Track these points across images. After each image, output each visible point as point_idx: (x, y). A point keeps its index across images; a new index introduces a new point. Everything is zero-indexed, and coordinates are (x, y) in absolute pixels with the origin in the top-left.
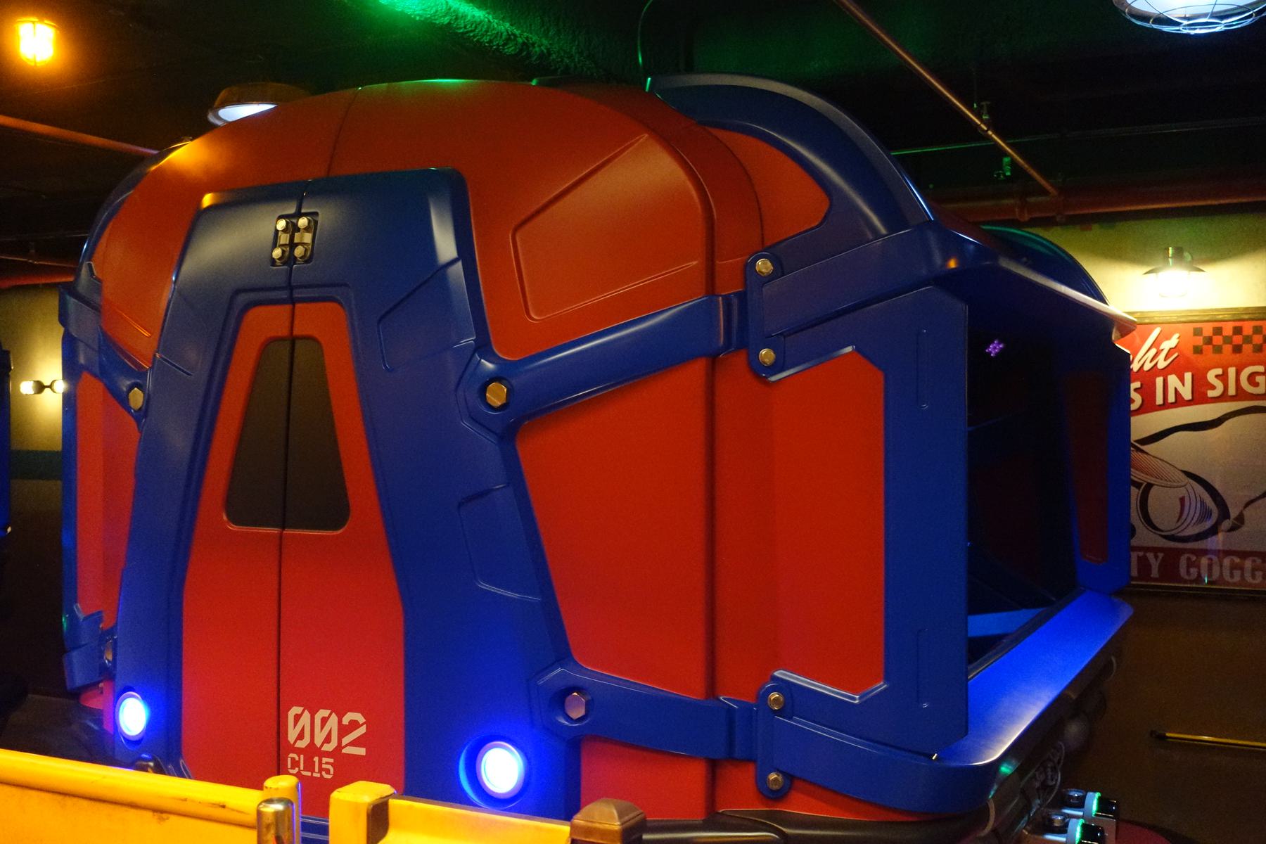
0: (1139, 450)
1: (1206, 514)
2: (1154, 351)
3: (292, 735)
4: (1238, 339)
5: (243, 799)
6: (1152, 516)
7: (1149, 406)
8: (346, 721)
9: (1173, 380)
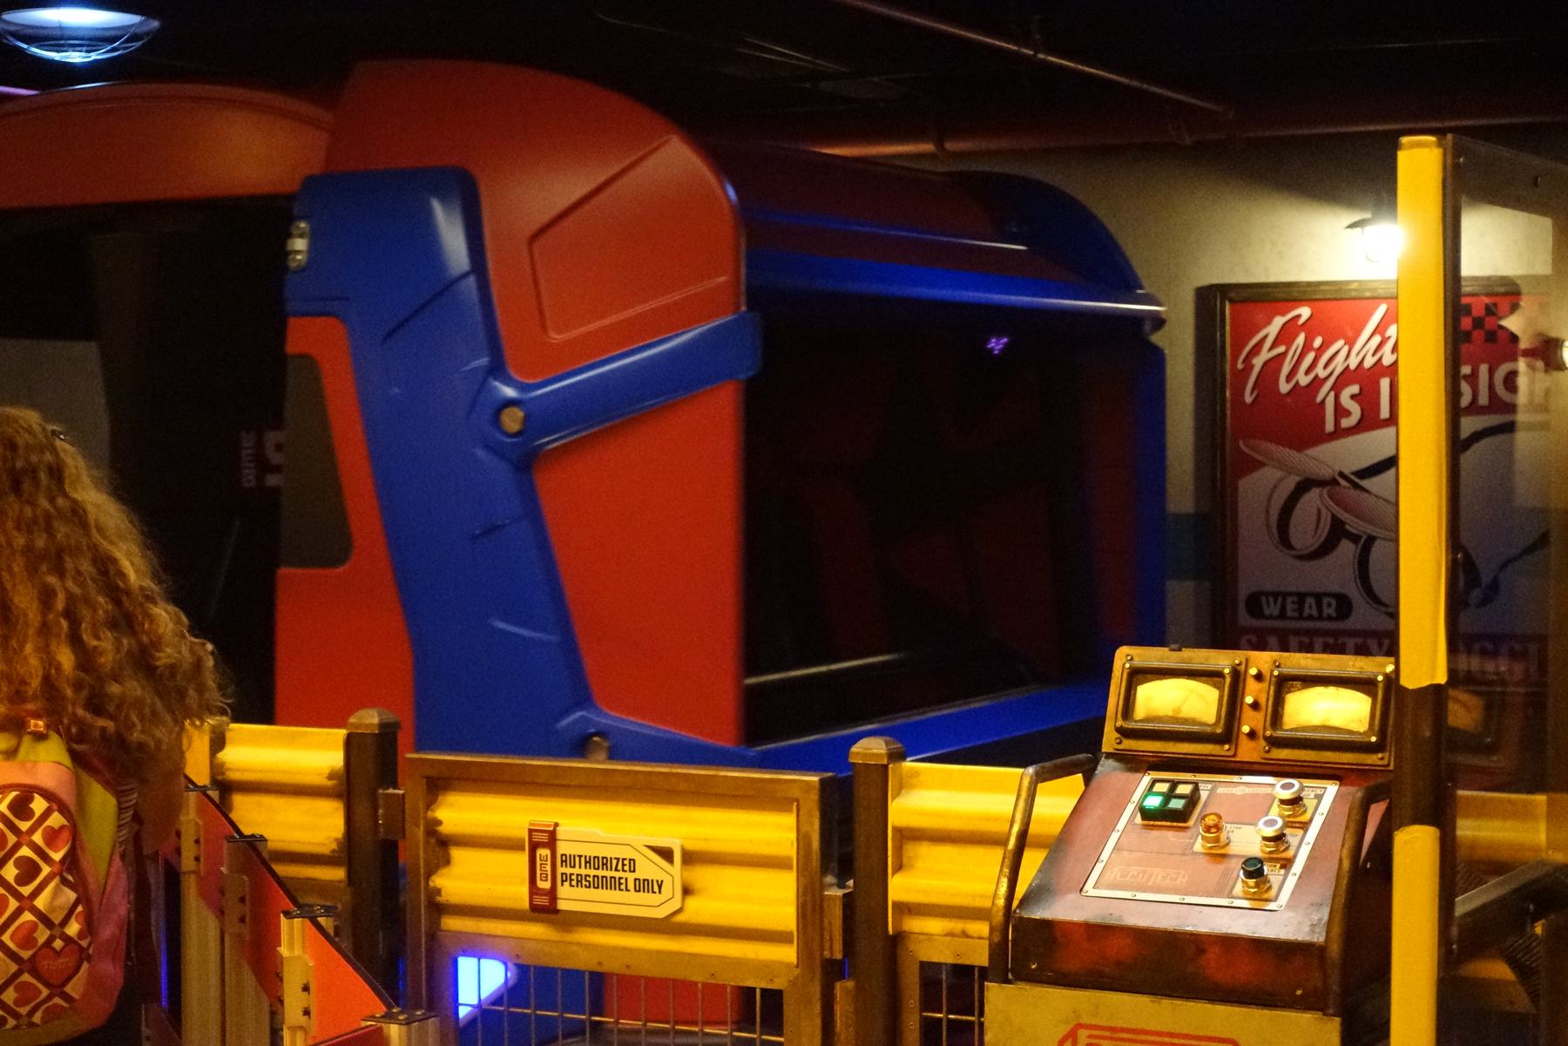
0: (1356, 486)
2: (1377, 339)
6: (1375, 586)
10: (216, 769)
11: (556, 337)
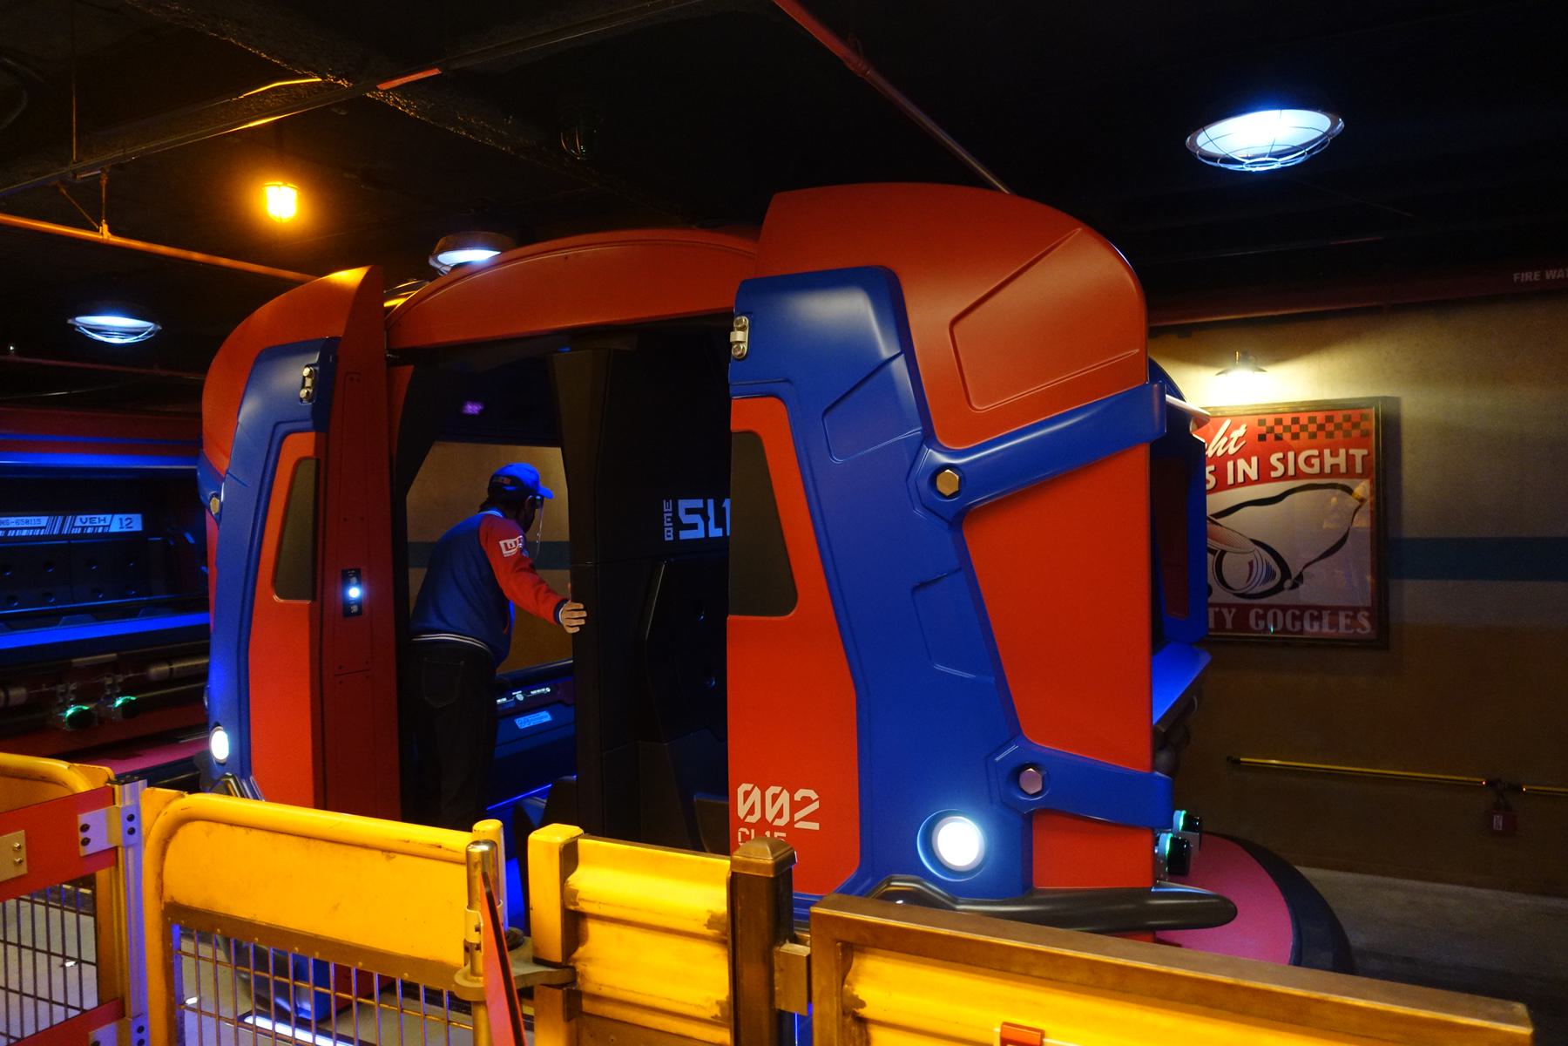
1: (1270, 574)
3: (742, 810)
4: (1296, 428)
5: (454, 840)
6: (1227, 580)
7: (1221, 485)
8: (798, 797)
9: (1242, 463)
10: (567, 896)
11: (981, 408)
